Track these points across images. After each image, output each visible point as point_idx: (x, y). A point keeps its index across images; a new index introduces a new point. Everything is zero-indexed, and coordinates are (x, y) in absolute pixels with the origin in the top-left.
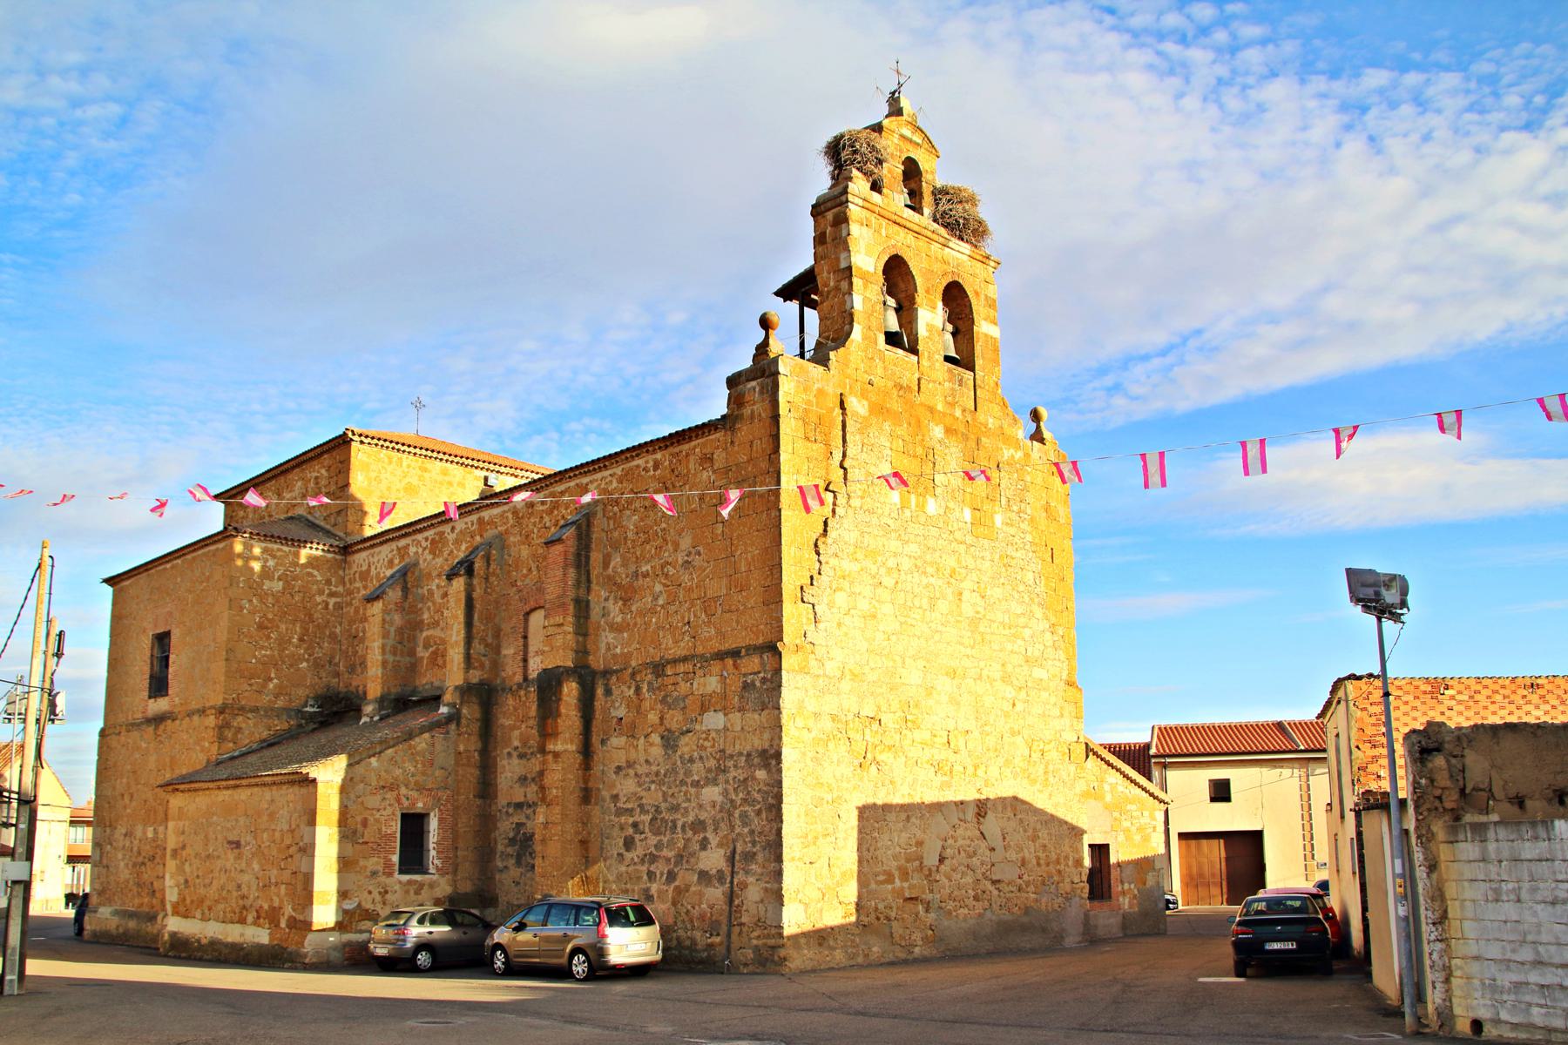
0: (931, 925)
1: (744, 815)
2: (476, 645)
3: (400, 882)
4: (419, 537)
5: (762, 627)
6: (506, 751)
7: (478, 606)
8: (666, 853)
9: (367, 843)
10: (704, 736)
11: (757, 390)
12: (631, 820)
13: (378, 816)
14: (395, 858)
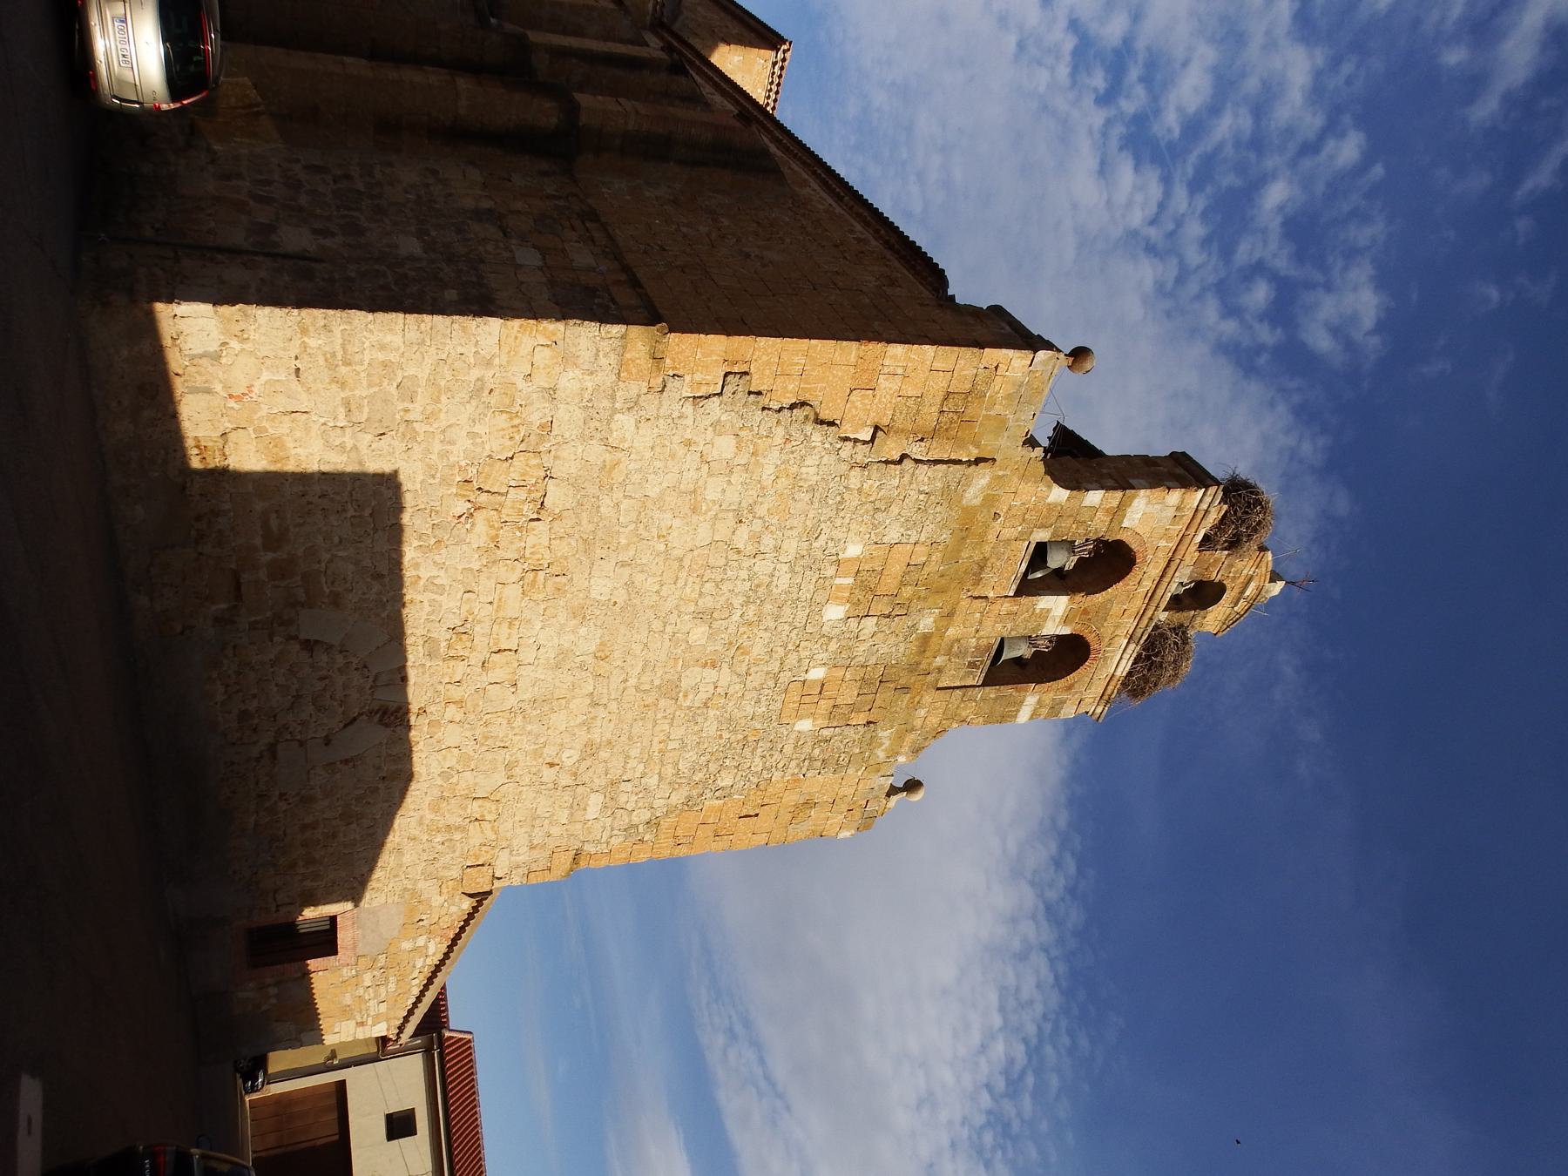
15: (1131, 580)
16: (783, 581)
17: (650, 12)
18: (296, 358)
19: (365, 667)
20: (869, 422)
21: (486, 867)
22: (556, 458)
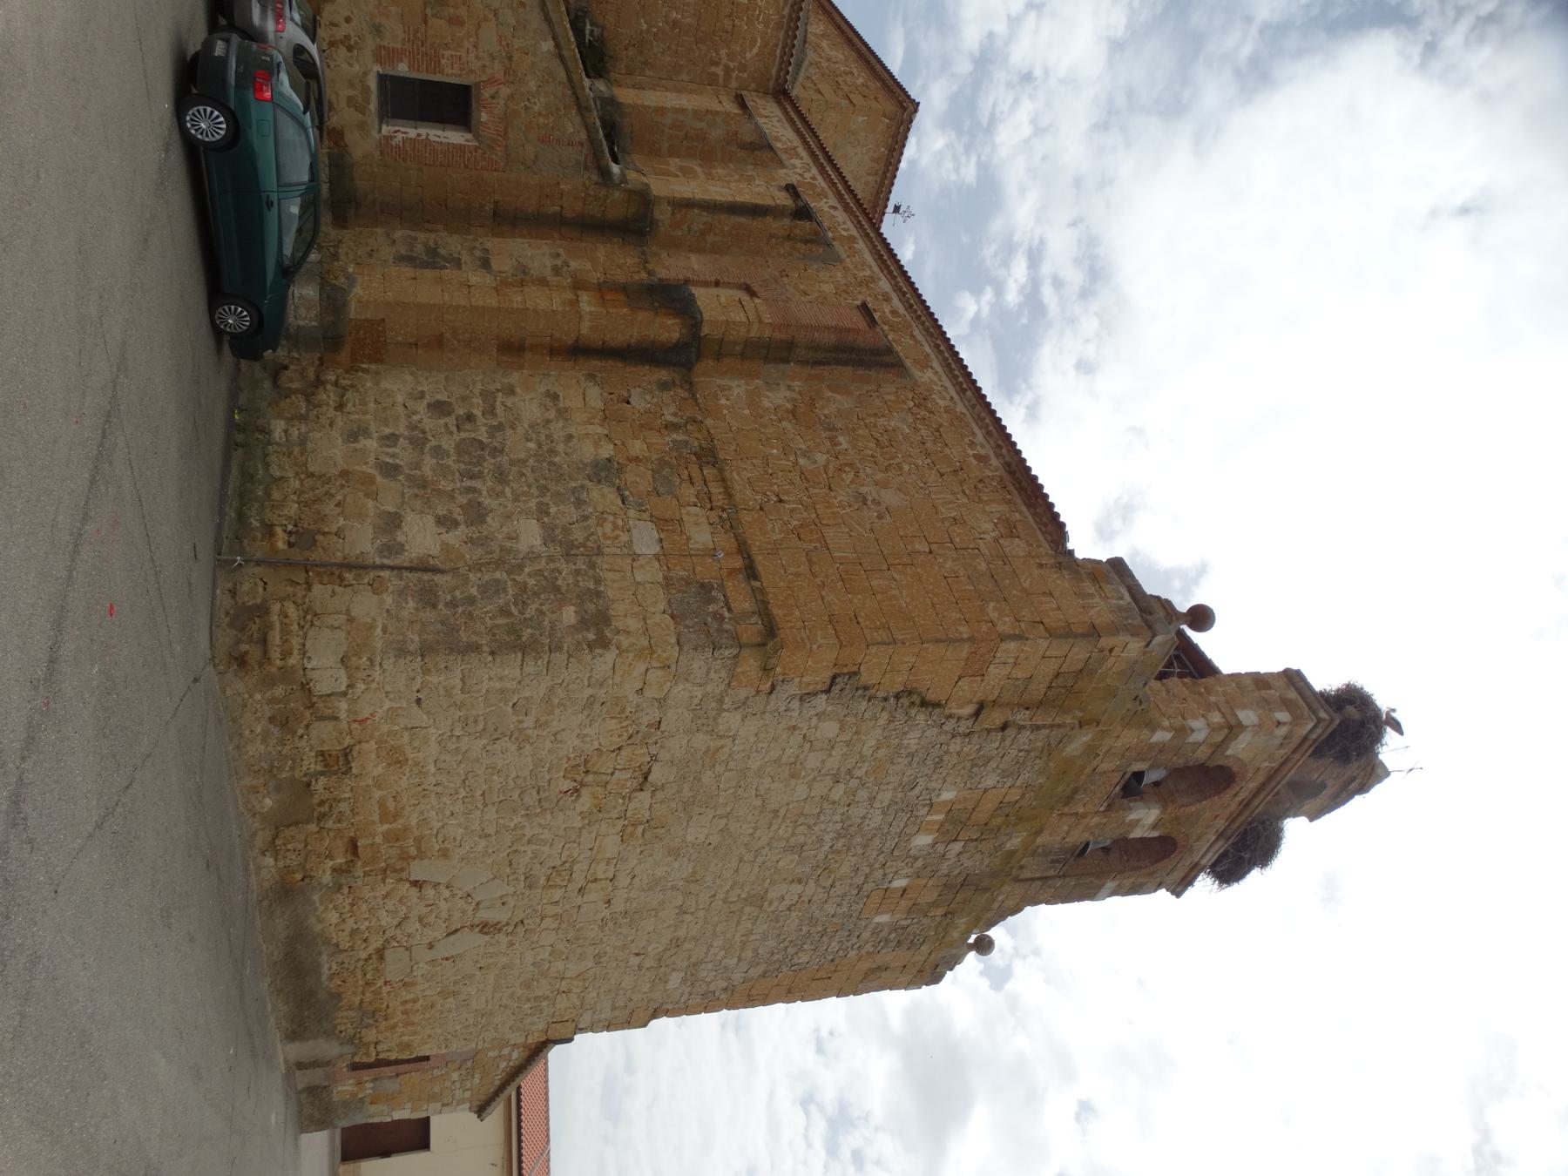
0: (312, 877)
1: (499, 587)
2: (706, 217)
3: (365, 74)
4: (814, 171)
5: (797, 613)
6: (561, 251)
7: (756, 224)
8: (429, 463)
9: (426, 22)
10: (620, 522)
11: (1121, 602)
12: (478, 412)
13: (466, 43)
14: (403, 69)
15: (1227, 796)
16: (876, 819)
17: (774, 76)
18: (418, 691)
19: (469, 895)
20: (974, 700)
21: (569, 1023)
22: (662, 747)
